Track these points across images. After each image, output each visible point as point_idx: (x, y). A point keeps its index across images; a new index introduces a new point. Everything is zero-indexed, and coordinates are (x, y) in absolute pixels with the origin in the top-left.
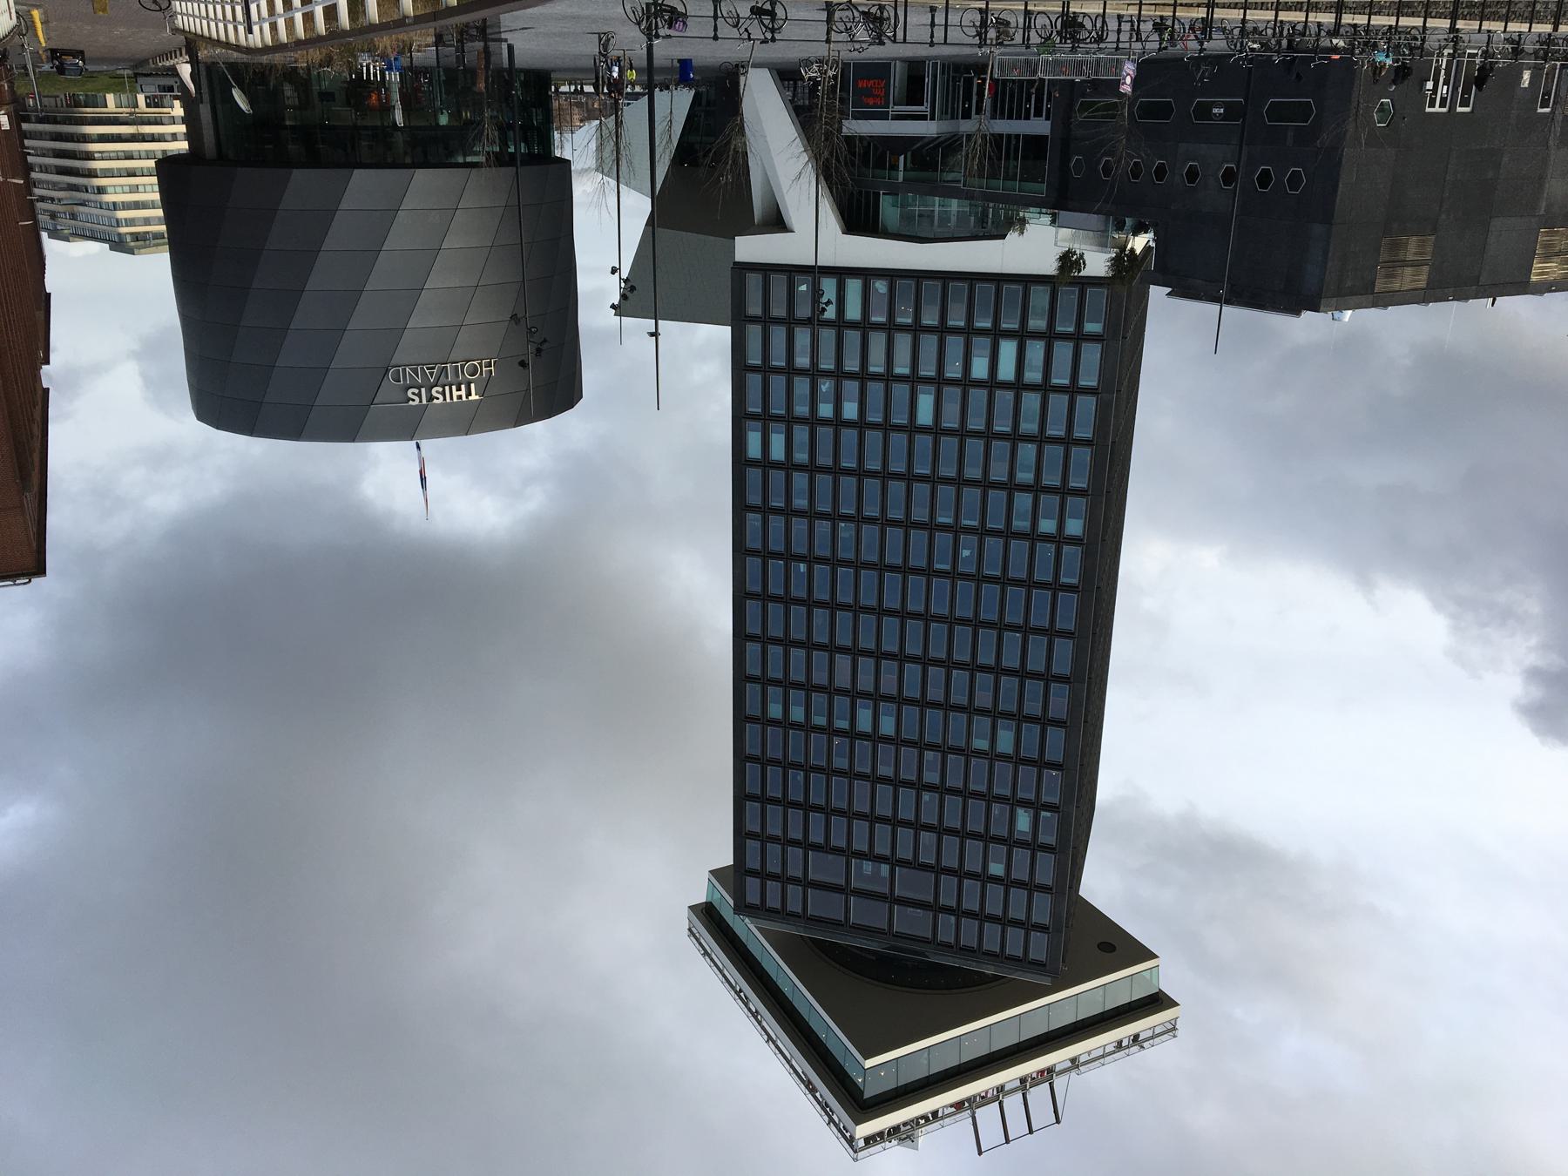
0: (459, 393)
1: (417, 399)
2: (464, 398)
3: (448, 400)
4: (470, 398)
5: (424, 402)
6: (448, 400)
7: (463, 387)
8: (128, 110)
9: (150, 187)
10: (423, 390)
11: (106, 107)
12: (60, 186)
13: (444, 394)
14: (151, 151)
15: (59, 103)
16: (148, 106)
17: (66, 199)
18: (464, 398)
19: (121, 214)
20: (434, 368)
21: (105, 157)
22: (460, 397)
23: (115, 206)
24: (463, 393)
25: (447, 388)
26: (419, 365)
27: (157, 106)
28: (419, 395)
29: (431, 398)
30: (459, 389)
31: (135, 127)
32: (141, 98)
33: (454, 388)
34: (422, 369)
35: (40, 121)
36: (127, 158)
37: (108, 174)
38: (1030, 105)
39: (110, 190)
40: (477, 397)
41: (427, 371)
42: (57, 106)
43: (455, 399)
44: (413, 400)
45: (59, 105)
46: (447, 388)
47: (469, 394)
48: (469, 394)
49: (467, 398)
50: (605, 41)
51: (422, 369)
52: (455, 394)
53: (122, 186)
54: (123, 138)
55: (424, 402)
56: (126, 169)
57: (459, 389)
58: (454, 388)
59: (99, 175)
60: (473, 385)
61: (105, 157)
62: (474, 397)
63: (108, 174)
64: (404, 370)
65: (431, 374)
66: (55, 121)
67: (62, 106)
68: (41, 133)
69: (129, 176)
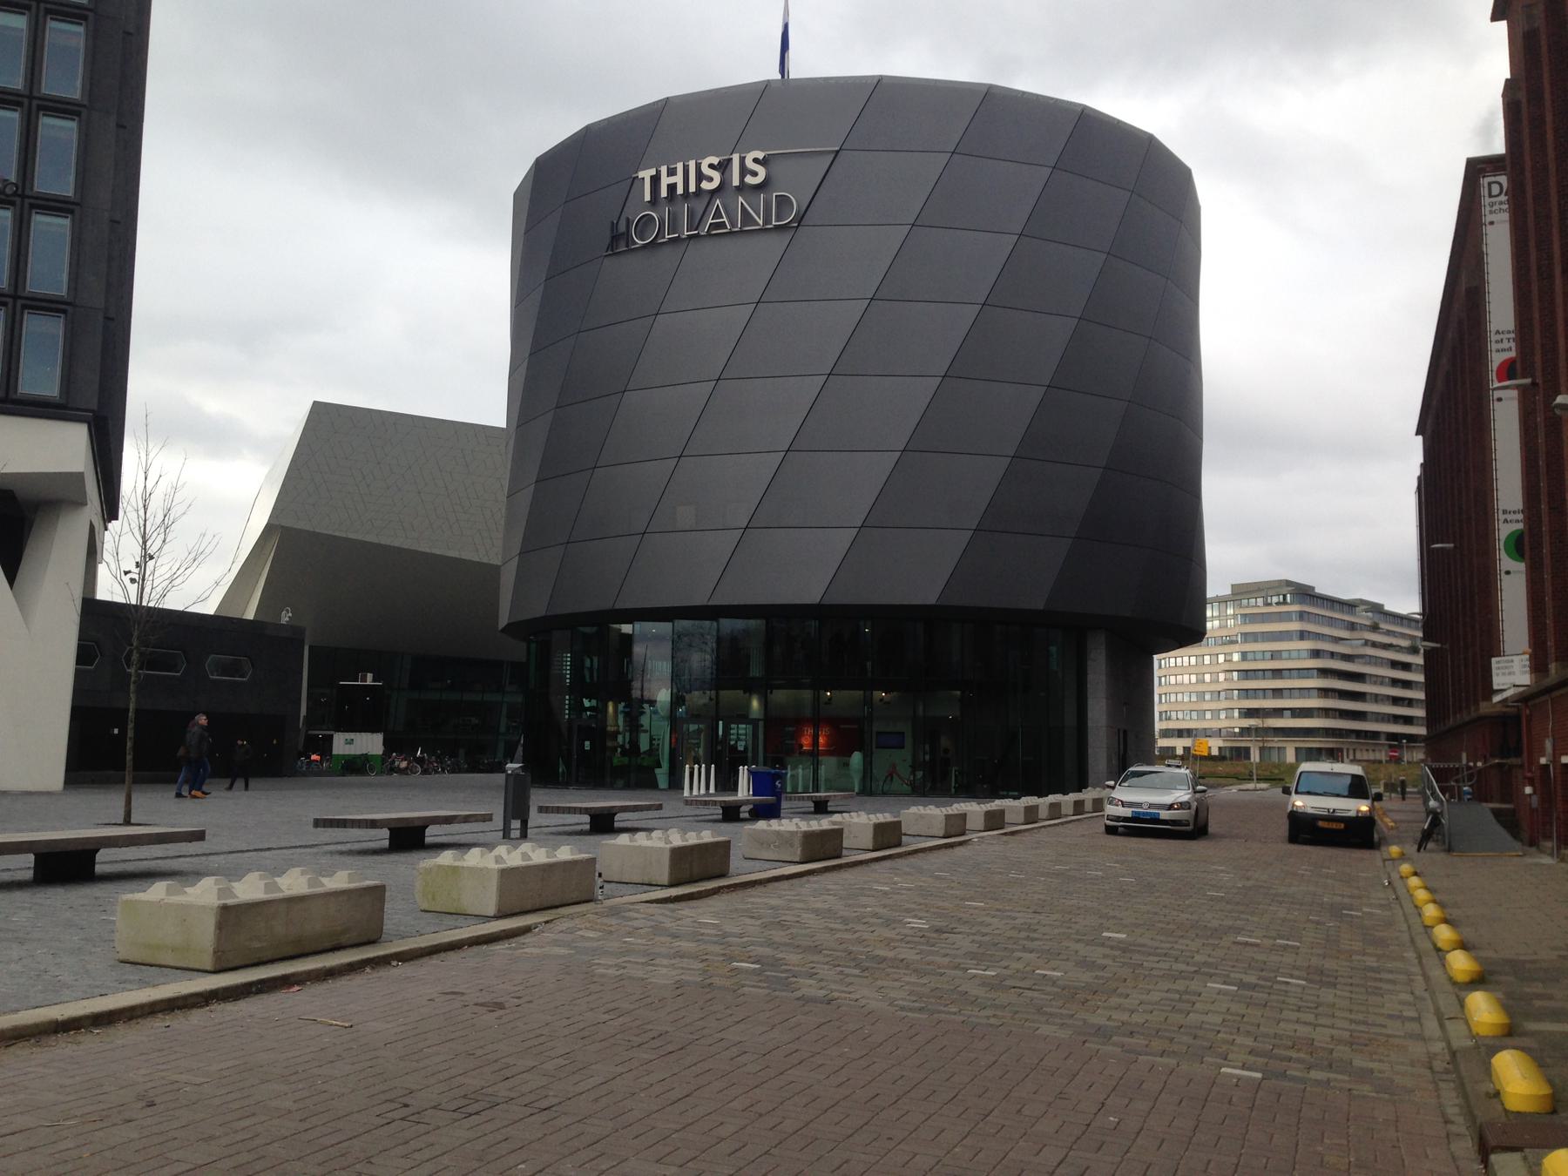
0: (672, 180)
1: (750, 164)
2: (664, 170)
3: (692, 164)
4: (653, 172)
5: (736, 158)
6: (692, 164)
7: (664, 193)
8: (1269, 745)
9: (1257, 658)
10: (736, 182)
11: (1296, 748)
12: (1364, 661)
13: (700, 177)
14: (1252, 698)
15: (1351, 752)
16: (1247, 750)
17: (1357, 647)
18: (664, 170)
19: (1295, 626)
20: (714, 226)
21: (1304, 692)
22: (672, 172)
23: (1302, 635)
24: (665, 181)
25: (692, 188)
26: (742, 231)
27: (1238, 749)
28: (744, 171)
29: (723, 167)
30: (672, 187)
31: (1265, 726)
32: (1255, 756)
33: (680, 190)
34: (733, 224)
35: (1375, 735)
36: (1280, 671)
37: (1302, 673)
38: (123, 731)
39: (1305, 654)
40: (641, 174)
41: (725, 219)
42: (1354, 750)
43: (680, 166)
44: (756, 160)
45: (1351, 752)
46: (692, 188)
47: (656, 180)
48: (656, 180)
49: (658, 172)
50: (464, 860)
51: (733, 224)
52: (678, 179)
53: (1290, 659)
54: (1401, 721)
55: (736, 158)
56: (1282, 698)
57: (672, 187)
58: (680, 190)
59: (1316, 671)
60: (647, 197)
61: (1304, 692)
62: (646, 174)
63: (1302, 673)
64: (767, 220)
65: (718, 214)
66: (1359, 734)
67: (1348, 750)
68: (1377, 721)
69: (1281, 689)
